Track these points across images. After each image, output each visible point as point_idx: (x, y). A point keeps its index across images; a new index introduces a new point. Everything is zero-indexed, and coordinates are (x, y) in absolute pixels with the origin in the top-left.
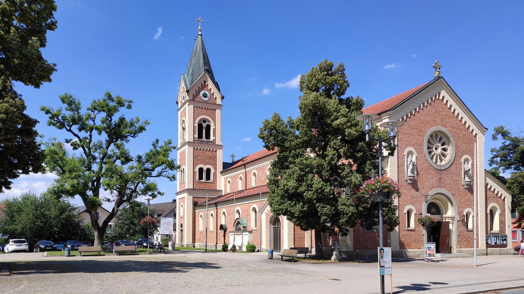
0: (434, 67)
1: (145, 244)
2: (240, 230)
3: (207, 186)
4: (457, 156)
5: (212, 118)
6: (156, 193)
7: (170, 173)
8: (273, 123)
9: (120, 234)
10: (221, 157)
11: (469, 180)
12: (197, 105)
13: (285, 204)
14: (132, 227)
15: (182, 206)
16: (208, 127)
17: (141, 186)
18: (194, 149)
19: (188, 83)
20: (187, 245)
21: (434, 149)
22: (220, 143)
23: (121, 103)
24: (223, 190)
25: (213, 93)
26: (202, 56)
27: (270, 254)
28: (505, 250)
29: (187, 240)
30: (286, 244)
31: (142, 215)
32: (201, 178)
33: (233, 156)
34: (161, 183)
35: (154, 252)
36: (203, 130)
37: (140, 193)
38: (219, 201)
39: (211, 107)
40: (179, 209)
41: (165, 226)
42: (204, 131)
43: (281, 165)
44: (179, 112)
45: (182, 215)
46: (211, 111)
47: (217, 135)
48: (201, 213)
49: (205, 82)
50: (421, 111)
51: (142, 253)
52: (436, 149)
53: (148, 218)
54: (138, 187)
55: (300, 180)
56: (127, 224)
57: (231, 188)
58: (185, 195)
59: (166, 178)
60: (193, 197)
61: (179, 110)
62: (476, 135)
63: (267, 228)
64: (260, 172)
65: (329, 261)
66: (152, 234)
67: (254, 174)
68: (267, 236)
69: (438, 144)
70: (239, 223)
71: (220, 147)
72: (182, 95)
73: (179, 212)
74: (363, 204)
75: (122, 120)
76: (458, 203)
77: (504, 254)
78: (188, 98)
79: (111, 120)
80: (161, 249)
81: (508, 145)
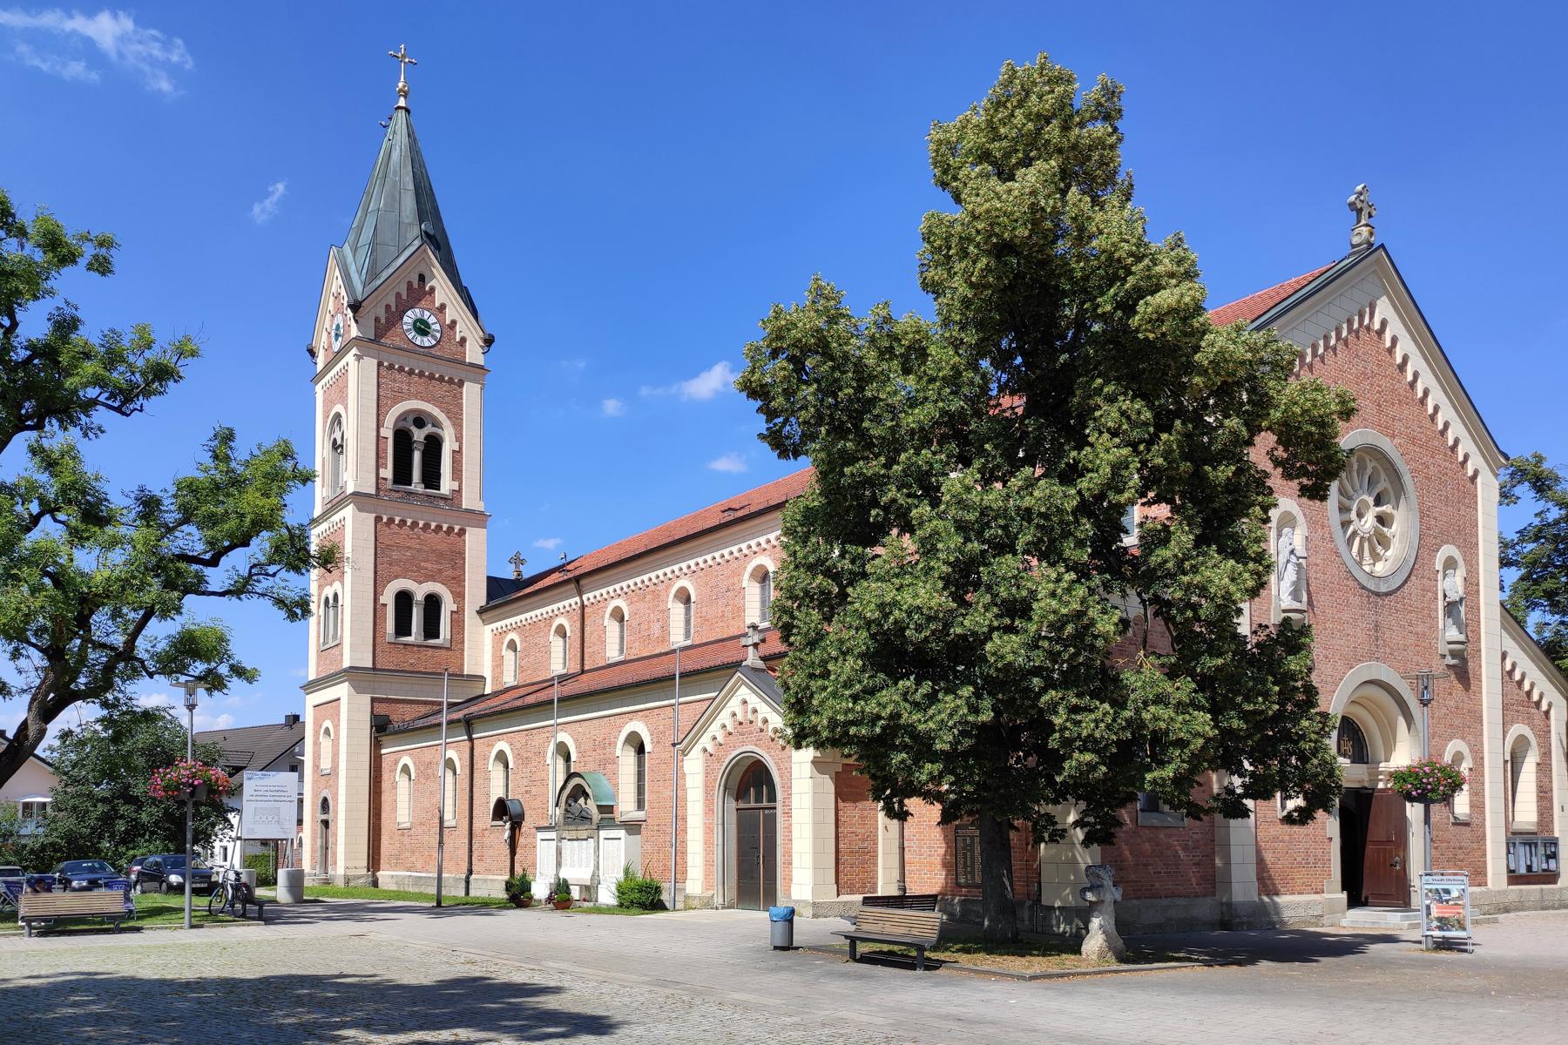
0: (1352, 205)
1: (174, 879)
2: (584, 818)
3: (426, 661)
4: (1425, 546)
5: (448, 413)
6: (223, 669)
7: (287, 582)
8: (808, 322)
9: (71, 838)
10: (481, 558)
11: (1462, 638)
12: (394, 359)
13: (884, 696)
14: (122, 809)
15: (327, 731)
16: (434, 444)
17: (159, 634)
18: (378, 519)
19: (353, 270)
20: (347, 880)
21: (1353, 515)
22: (479, 506)
23: (59, 251)
24: (487, 674)
25: (454, 322)
26: (411, 186)
27: (781, 926)
28: (1553, 892)
29: (347, 858)
30: (803, 872)
31: (162, 756)
32: (403, 627)
33: (518, 560)
34: (245, 626)
35: (212, 916)
36: (413, 456)
37: (150, 664)
38: (476, 715)
39: (446, 370)
40: (316, 743)
41: (262, 804)
42: (417, 457)
43: (846, 518)
44: (318, 388)
45: (326, 765)
46: (446, 387)
47: (467, 473)
48: (406, 760)
49: (422, 278)
50: (1317, 364)
51: (157, 921)
52: (1360, 515)
53: (184, 770)
54: (140, 642)
55: (962, 578)
56: (104, 800)
57: (519, 669)
58: (342, 690)
59: (267, 603)
60: (373, 700)
61: (316, 378)
62: (1476, 473)
63: (708, 811)
65: (1068, 960)
66: (204, 837)
67: (618, 615)
68: (708, 844)
69: (1365, 497)
70: (580, 792)
71: (479, 518)
72: (333, 320)
73: (317, 756)
74: (1248, 699)
75: (66, 326)
77: (1554, 908)
78: (354, 331)
79: (14, 324)
80: (249, 899)
81: (1557, 522)
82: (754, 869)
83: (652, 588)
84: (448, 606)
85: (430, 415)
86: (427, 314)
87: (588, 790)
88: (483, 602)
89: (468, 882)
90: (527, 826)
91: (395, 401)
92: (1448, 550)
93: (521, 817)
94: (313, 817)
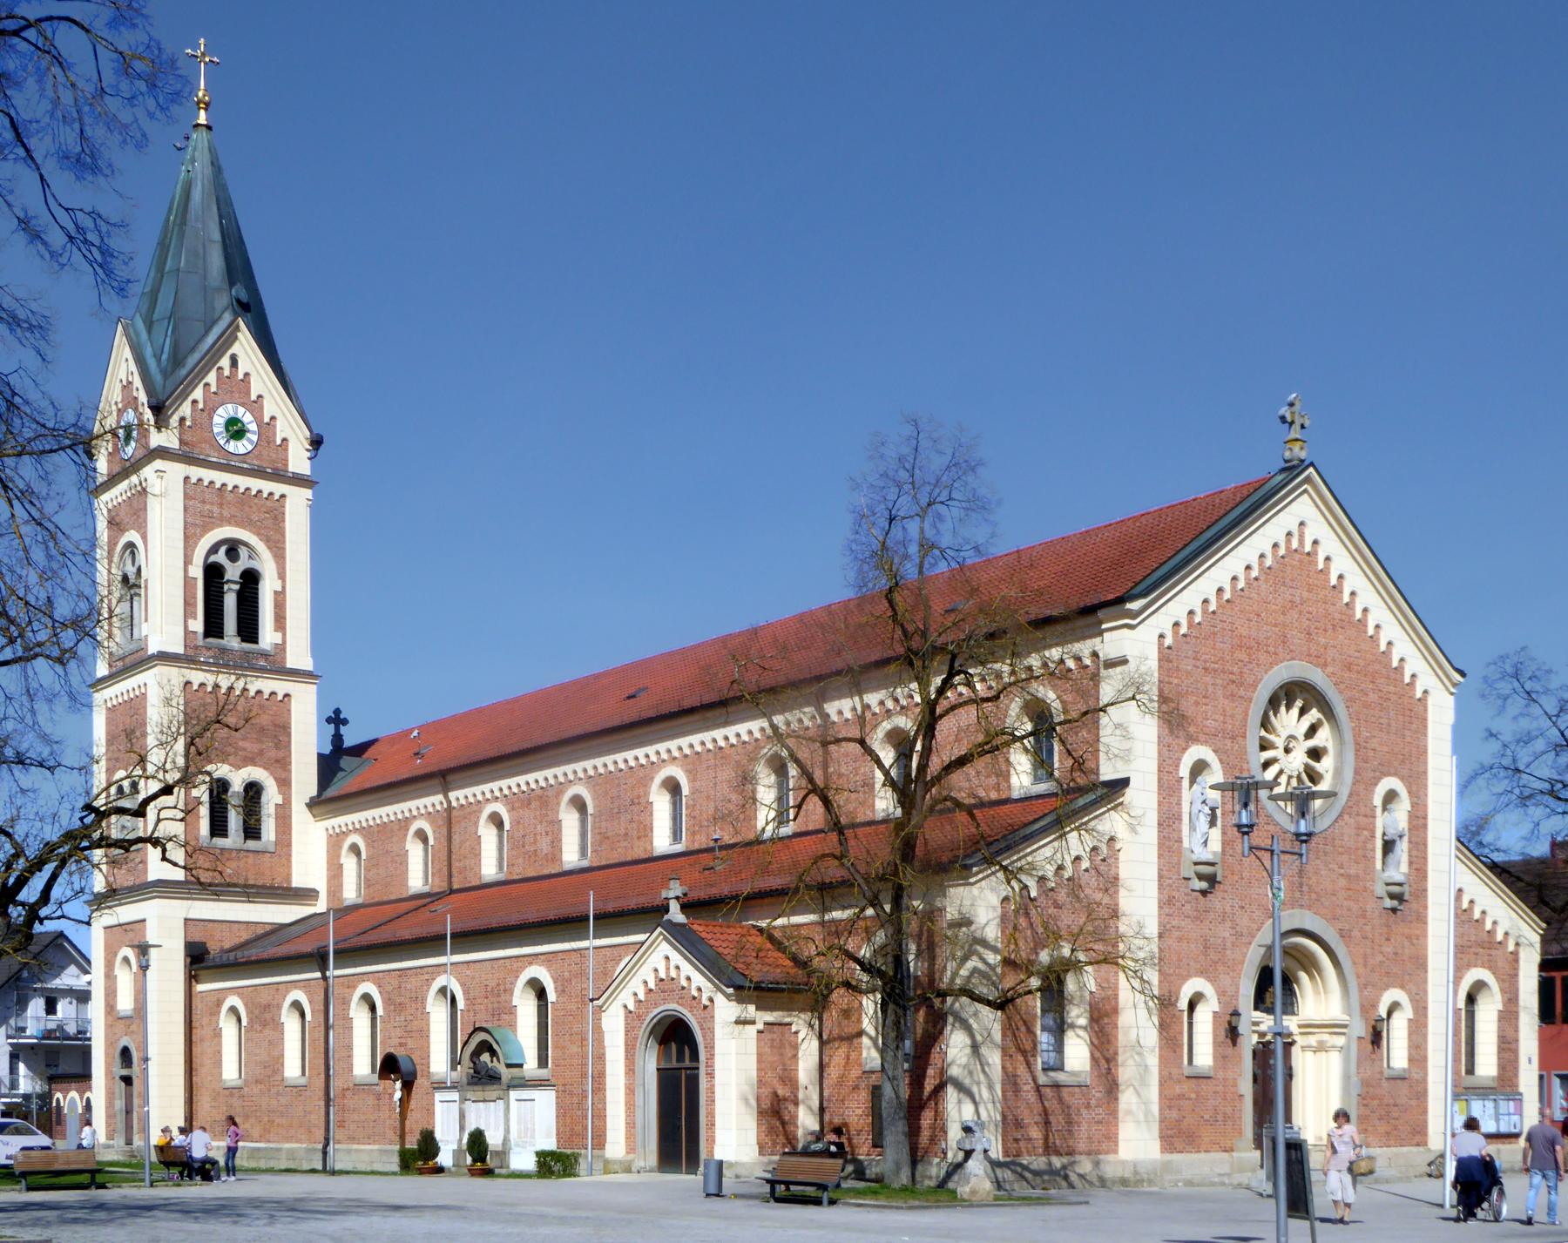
5: (268, 541)
16: (250, 579)
26: (217, 236)
30: (733, 1135)
40: (110, 977)
45: (125, 1003)
48: (234, 1000)
57: (367, 882)
64: (527, 814)
76: (1361, 970)
82: (679, 1129)
83: (540, 792)
84: (271, 797)
85: (246, 544)
86: (241, 410)
87: (495, 1046)
88: (314, 791)
89: (325, 1153)
90: (420, 1084)
91: (206, 528)
92: (1389, 783)
93: (414, 1075)
94: (108, 1072)
